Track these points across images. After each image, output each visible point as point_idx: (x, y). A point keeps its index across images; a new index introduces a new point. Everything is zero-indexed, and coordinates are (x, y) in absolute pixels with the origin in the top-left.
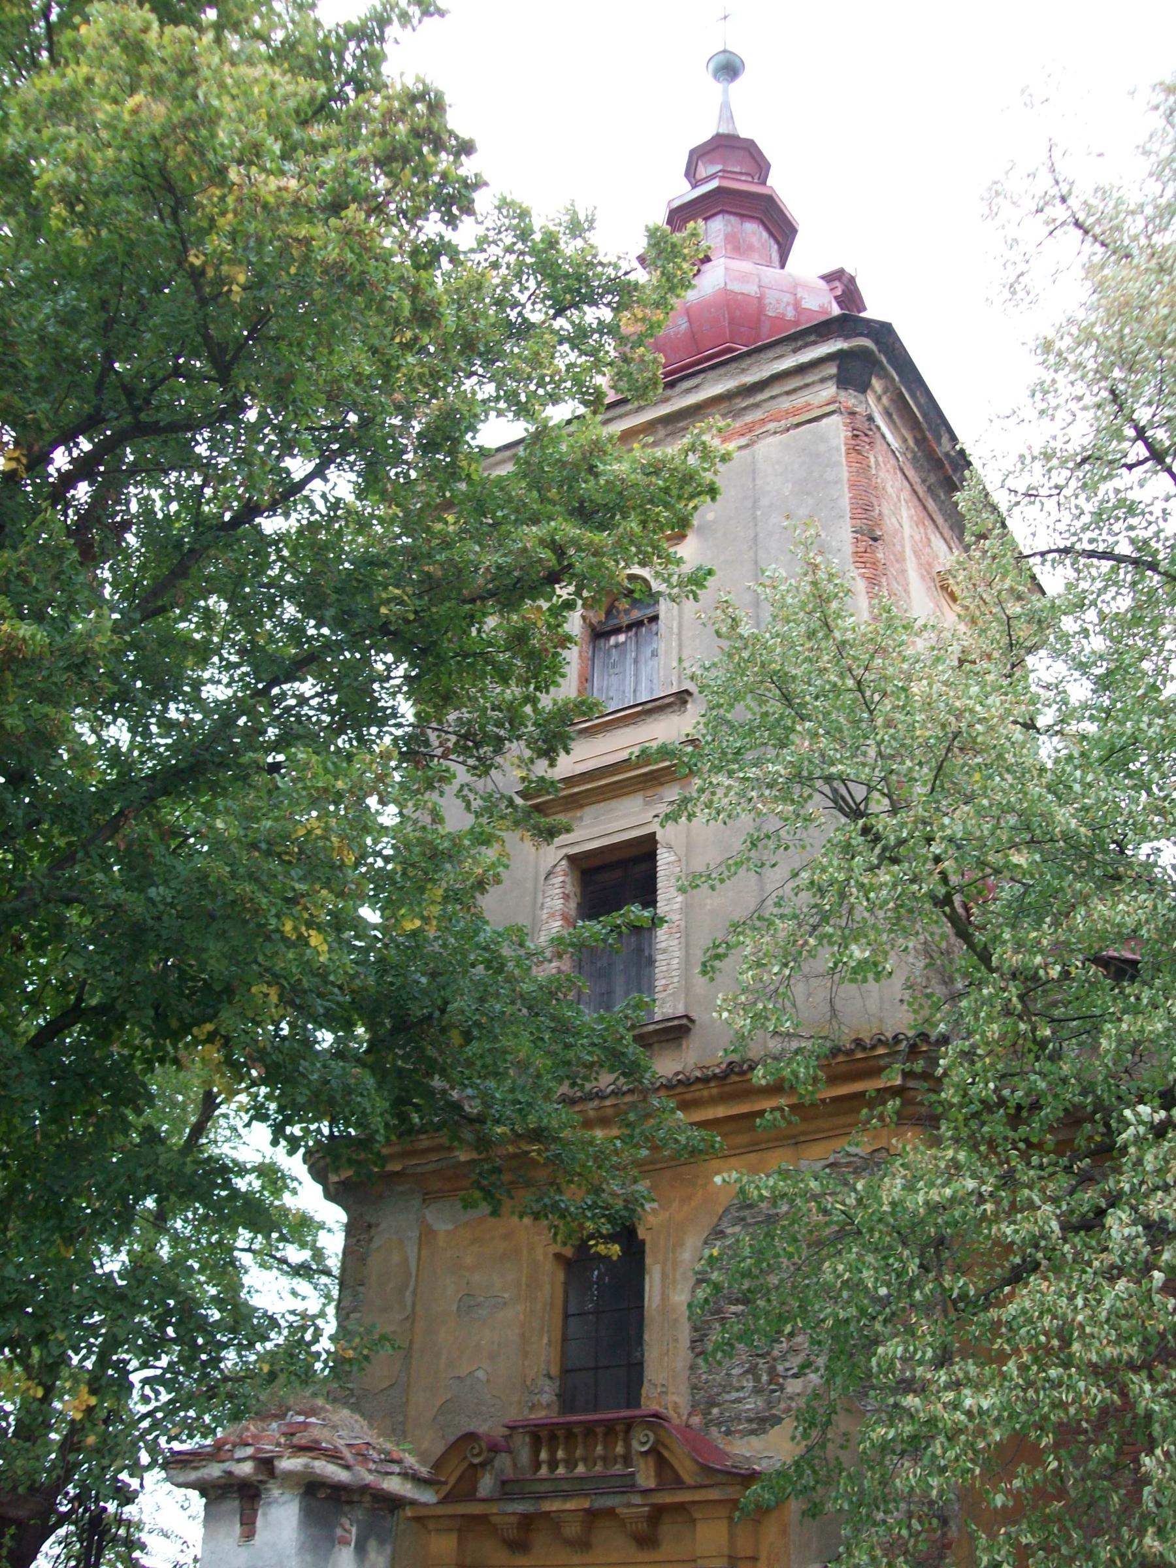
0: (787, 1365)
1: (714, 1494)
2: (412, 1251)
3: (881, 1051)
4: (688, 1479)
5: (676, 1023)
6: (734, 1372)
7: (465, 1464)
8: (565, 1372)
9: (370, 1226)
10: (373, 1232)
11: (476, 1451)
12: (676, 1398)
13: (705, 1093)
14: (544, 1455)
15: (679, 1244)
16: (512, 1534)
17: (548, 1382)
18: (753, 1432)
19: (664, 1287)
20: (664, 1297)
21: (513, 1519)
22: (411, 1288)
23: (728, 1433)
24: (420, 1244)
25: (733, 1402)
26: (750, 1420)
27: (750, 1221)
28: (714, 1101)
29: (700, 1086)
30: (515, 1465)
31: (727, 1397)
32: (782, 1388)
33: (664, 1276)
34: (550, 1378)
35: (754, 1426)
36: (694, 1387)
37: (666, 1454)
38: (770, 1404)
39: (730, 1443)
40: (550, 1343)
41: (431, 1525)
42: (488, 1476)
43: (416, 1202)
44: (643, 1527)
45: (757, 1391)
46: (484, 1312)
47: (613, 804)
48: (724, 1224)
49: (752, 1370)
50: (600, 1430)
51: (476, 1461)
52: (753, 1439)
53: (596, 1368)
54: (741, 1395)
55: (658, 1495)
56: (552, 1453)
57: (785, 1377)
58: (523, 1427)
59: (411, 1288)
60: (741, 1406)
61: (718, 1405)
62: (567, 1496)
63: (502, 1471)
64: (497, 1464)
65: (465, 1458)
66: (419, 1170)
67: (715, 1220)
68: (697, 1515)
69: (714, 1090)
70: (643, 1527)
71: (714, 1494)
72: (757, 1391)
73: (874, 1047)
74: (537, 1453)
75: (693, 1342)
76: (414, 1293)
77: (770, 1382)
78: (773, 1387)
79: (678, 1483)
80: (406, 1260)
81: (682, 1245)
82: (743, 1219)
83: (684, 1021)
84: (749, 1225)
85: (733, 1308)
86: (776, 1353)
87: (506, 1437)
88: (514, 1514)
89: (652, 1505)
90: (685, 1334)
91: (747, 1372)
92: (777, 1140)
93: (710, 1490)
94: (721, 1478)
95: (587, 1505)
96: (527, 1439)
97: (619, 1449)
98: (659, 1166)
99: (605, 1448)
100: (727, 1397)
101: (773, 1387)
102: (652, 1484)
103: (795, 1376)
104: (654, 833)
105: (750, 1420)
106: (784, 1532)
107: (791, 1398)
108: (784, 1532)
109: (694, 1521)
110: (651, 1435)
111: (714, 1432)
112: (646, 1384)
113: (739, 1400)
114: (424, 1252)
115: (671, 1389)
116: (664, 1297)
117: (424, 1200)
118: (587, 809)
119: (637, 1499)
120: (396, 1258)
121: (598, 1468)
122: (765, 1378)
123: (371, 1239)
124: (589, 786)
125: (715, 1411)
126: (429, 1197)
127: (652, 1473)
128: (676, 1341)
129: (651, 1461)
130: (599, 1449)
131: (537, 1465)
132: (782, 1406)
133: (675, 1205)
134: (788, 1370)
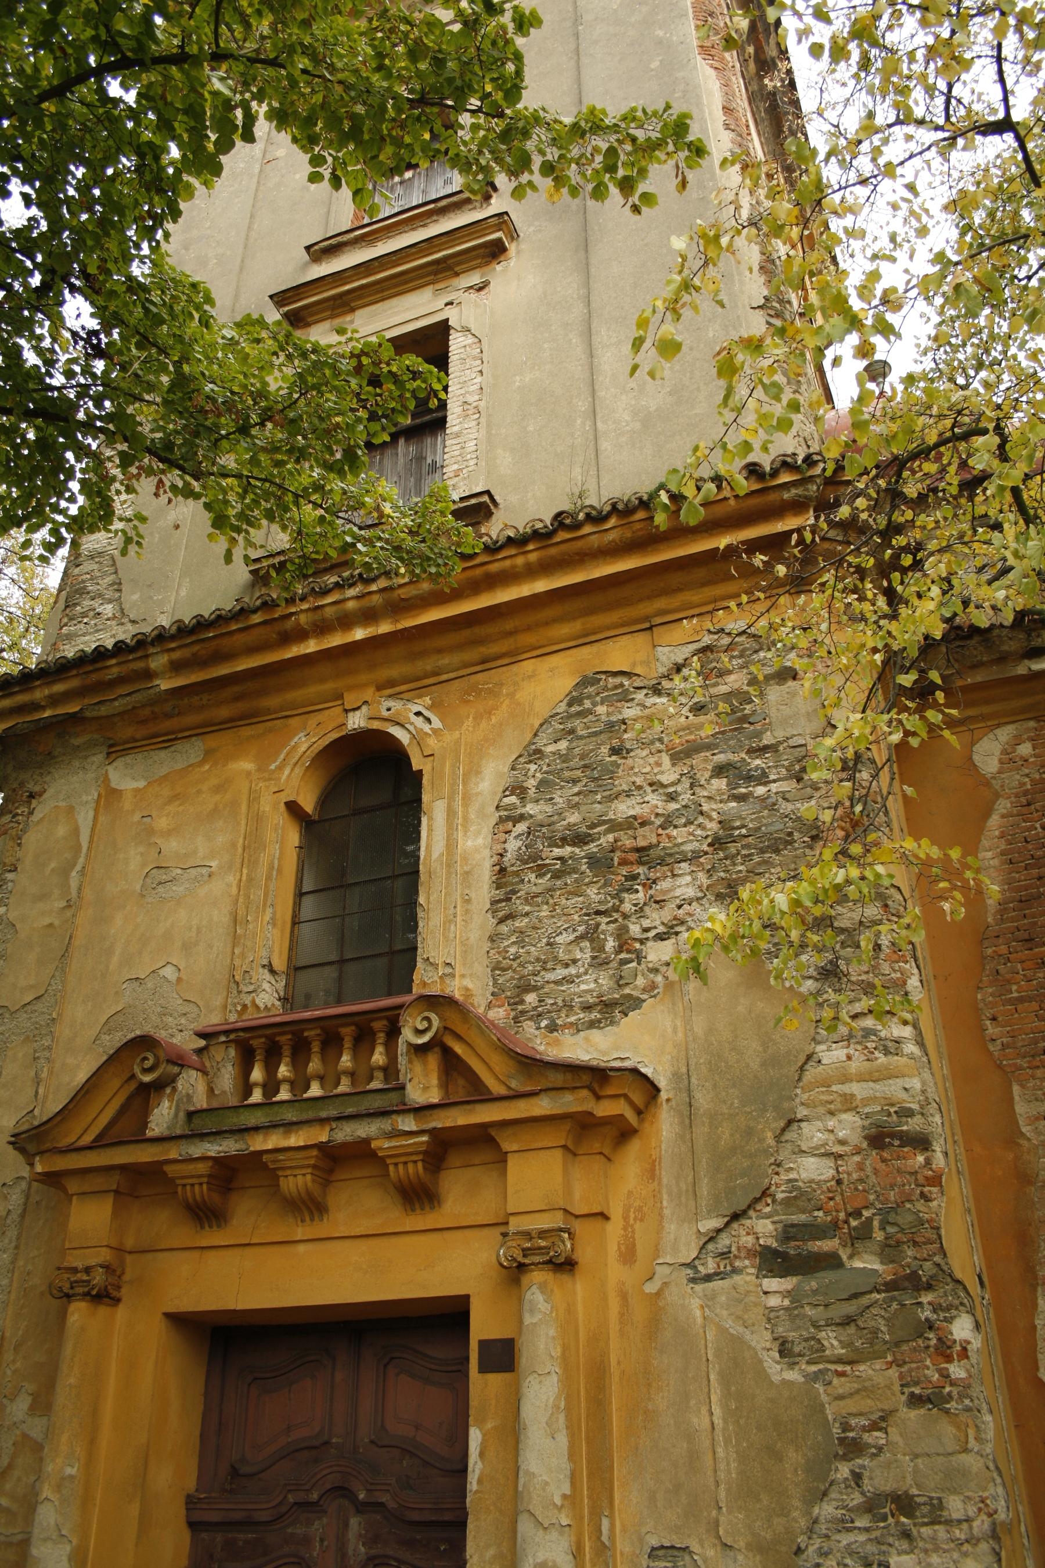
0: (646, 923)
1: (542, 1106)
2: (85, 818)
3: (785, 478)
4: (496, 1088)
5: (473, 501)
6: (559, 939)
7: (133, 1086)
8: (295, 969)
9: (32, 796)
10: (34, 802)
11: (148, 1064)
12: (468, 983)
13: (520, 561)
14: (257, 1074)
15: (474, 771)
16: (201, 1192)
17: (267, 976)
18: (592, 1025)
19: (451, 827)
20: (451, 844)
21: (202, 1168)
22: (78, 867)
23: (552, 1028)
24: (96, 811)
25: (556, 983)
26: (587, 1008)
27: (581, 733)
28: (531, 572)
29: (513, 551)
30: (211, 1091)
31: (550, 976)
32: (639, 957)
33: (451, 813)
34: (272, 972)
35: (595, 1015)
36: (497, 967)
37: (458, 1049)
38: (620, 982)
39: (557, 1042)
40: (273, 922)
41: (73, 1186)
42: (166, 1103)
43: (99, 758)
44: (416, 1170)
45: (599, 963)
46: (179, 889)
47: (394, 301)
48: (541, 741)
49: (591, 935)
50: (347, 1032)
51: (147, 1078)
52: (595, 1035)
53: (342, 962)
54: (573, 970)
55: (442, 1113)
56: (271, 1069)
57: (642, 942)
58: (226, 1032)
59: (78, 867)
60: (573, 988)
61: (535, 989)
62: (289, 1126)
63: (189, 1097)
64: (180, 1084)
65: (133, 1076)
66: (104, 711)
67: (528, 736)
68: (506, 1146)
69: (533, 555)
70: (416, 1170)
71: (542, 1106)
72: (599, 963)
73: (775, 473)
74: (247, 1071)
75: (494, 903)
76: (83, 872)
77: (619, 950)
78: (623, 956)
79: (481, 1095)
80: (76, 831)
81: (478, 773)
82: (572, 731)
83: (485, 498)
84: (581, 738)
85: (557, 852)
86: (627, 907)
87: (199, 1051)
88: (203, 1159)
89: (432, 1132)
90: (483, 891)
91: (582, 937)
92: (623, 625)
93: (534, 1101)
94: (557, 1078)
95: (324, 1138)
96: (232, 1052)
97: (379, 1057)
98: (445, 677)
99: (355, 1057)
100: (550, 976)
101: (623, 956)
102: (434, 1097)
103: (661, 937)
104: (447, 320)
105: (587, 1008)
106: (652, 1173)
107: (656, 971)
108: (652, 1173)
109: (502, 1159)
110: (434, 1017)
111: (529, 1027)
112: (420, 964)
113: (569, 980)
114: (101, 819)
115: (459, 970)
116: (451, 844)
117: (109, 754)
118: (359, 313)
119: (408, 1123)
120: (61, 831)
121: (344, 1087)
122: (610, 944)
123: (31, 813)
124: (364, 282)
125: (531, 998)
126: (115, 750)
127: (435, 1081)
128: (468, 901)
129: (433, 1060)
130: (346, 1060)
131: (247, 1089)
132: (640, 981)
133: (469, 722)
134: (646, 930)
